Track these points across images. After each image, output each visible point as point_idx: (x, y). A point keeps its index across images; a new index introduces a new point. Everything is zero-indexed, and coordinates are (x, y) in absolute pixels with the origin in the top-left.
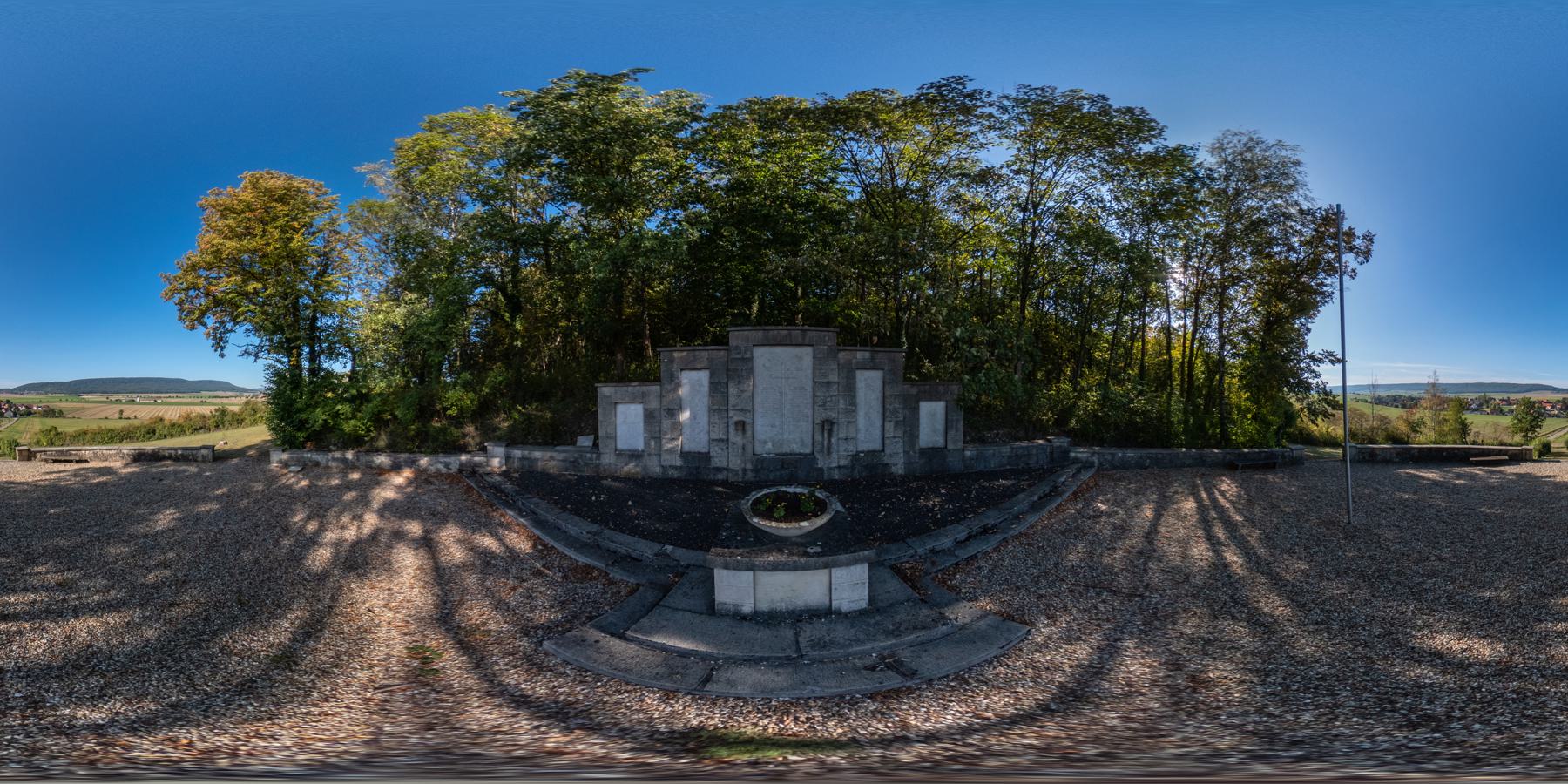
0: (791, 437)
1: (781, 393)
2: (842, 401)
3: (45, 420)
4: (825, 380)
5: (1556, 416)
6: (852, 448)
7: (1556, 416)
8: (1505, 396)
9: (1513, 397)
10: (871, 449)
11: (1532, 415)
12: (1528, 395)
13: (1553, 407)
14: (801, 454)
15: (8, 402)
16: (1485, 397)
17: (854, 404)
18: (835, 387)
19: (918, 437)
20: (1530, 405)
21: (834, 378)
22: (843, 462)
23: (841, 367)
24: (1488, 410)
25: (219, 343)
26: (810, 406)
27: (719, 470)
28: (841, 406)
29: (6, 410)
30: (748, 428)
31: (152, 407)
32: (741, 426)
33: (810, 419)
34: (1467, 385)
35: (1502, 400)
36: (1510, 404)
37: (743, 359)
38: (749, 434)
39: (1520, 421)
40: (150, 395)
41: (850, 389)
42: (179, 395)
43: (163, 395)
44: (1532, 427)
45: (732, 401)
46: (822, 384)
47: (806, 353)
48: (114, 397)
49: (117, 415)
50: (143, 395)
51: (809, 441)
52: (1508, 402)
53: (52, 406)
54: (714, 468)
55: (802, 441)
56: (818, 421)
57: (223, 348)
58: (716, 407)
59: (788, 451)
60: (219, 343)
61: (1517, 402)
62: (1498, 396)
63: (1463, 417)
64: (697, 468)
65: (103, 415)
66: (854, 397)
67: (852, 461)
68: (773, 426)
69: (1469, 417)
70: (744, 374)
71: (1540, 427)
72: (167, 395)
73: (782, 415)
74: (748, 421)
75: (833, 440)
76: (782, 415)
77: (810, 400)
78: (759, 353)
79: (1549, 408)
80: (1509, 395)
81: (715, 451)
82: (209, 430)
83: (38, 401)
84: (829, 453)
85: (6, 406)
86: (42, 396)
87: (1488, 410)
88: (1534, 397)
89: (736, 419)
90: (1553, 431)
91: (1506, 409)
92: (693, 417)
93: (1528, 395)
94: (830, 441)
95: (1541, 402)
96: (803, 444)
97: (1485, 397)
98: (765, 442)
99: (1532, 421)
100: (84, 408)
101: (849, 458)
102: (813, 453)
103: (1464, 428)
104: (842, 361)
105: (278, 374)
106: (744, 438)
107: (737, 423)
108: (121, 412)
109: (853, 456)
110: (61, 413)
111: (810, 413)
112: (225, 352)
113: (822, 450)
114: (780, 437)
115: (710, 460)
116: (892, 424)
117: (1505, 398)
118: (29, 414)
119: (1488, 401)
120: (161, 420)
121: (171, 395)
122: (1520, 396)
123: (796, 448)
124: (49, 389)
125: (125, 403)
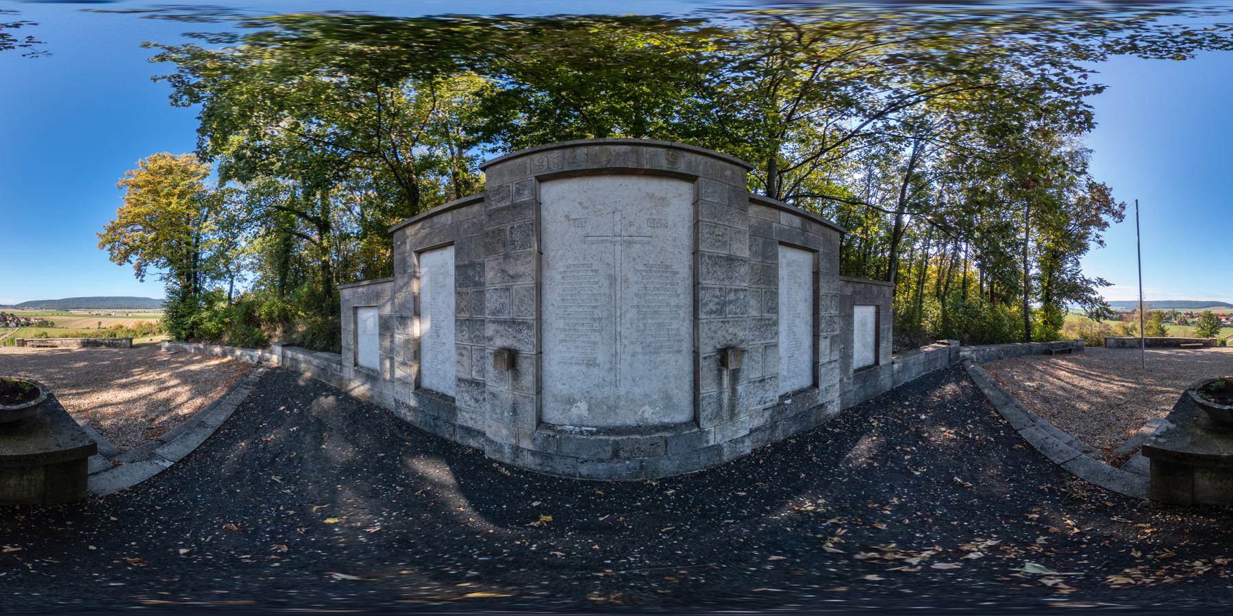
0: (637, 390)
1: (612, 280)
2: (753, 302)
3: (40, 329)
4: (723, 252)
5: (1229, 326)
6: (772, 396)
7: (1229, 326)
8: (1189, 311)
9: (1195, 311)
10: (797, 387)
11: (1213, 323)
12: (1209, 309)
13: (1227, 319)
14: (665, 427)
15: (12, 315)
16: (1173, 311)
17: (774, 309)
18: (744, 270)
19: (852, 357)
20: (1210, 316)
21: (742, 249)
22: (758, 422)
23: (755, 233)
24: (1176, 322)
25: (140, 273)
26: (685, 312)
27: (469, 431)
28: (753, 313)
29: (10, 321)
30: (526, 366)
31: (86, 319)
32: (510, 359)
33: (687, 346)
34: (1159, 302)
35: (1187, 314)
36: (1193, 317)
37: (514, 206)
38: (528, 380)
39: (1203, 328)
40: (123, 310)
41: (767, 277)
42: (146, 310)
43: (133, 310)
44: (1212, 333)
45: (492, 300)
46: (716, 260)
47: (678, 196)
48: (95, 312)
49: (97, 326)
50: (118, 310)
51: (683, 397)
52: (1192, 316)
53: (46, 318)
54: (462, 427)
55: (667, 398)
56: (707, 349)
57: (143, 276)
58: (466, 315)
59: (631, 421)
60: (140, 273)
61: (1199, 315)
62: (1183, 311)
63: (1162, 325)
64: (436, 419)
65: (85, 326)
66: (774, 294)
67: (772, 417)
68: (591, 363)
69: (1167, 326)
70: (517, 236)
71: (1218, 333)
72: (137, 310)
73: (616, 337)
74: (527, 350)
75: (740, 389)
76: (616, 337)
77: (685, 300)
78: (552, 192)
79: (1223, 320)
80: (1192, 310)
81: (464, 400)
82: (155, 334)
83: (34, 314)
84: (733, 415)
85: (11, 319)
86: (37, 311)
87: (1176, 322)
88: (1214, 311)
89: (499, 342)
90: (1223, 334)
91: (1190, 321)
92: (436, 329)
93: (1209, 309)
94: (734, 391)
95: (1217, 315)
96: (668, 402)
97: (1173, 311)
98: (571, 401)
99: (1212, 329)
100: (70, 321)
101: (767, 414)
102: (696, 420)
103: (1163, 332)
104: (753, 222)
105: (173, 292)
106: (515, 388)
107: (499, 353)
108: (100, 323)
109: (773, 407)
110: (53, 324)
111: (685, 329)
112: (144, 279)
113: (717, 415)
114: (607, 390)
115: (455, 414)
116: (828, 341)
117: (1189, 312)
118: (28, 325)
119: (1175, 315)
120: (121, 327)
121: (140, 310)
122: (1202, 311)
123: (650, 415)
124: (43, 306)
125: (102, 317)
